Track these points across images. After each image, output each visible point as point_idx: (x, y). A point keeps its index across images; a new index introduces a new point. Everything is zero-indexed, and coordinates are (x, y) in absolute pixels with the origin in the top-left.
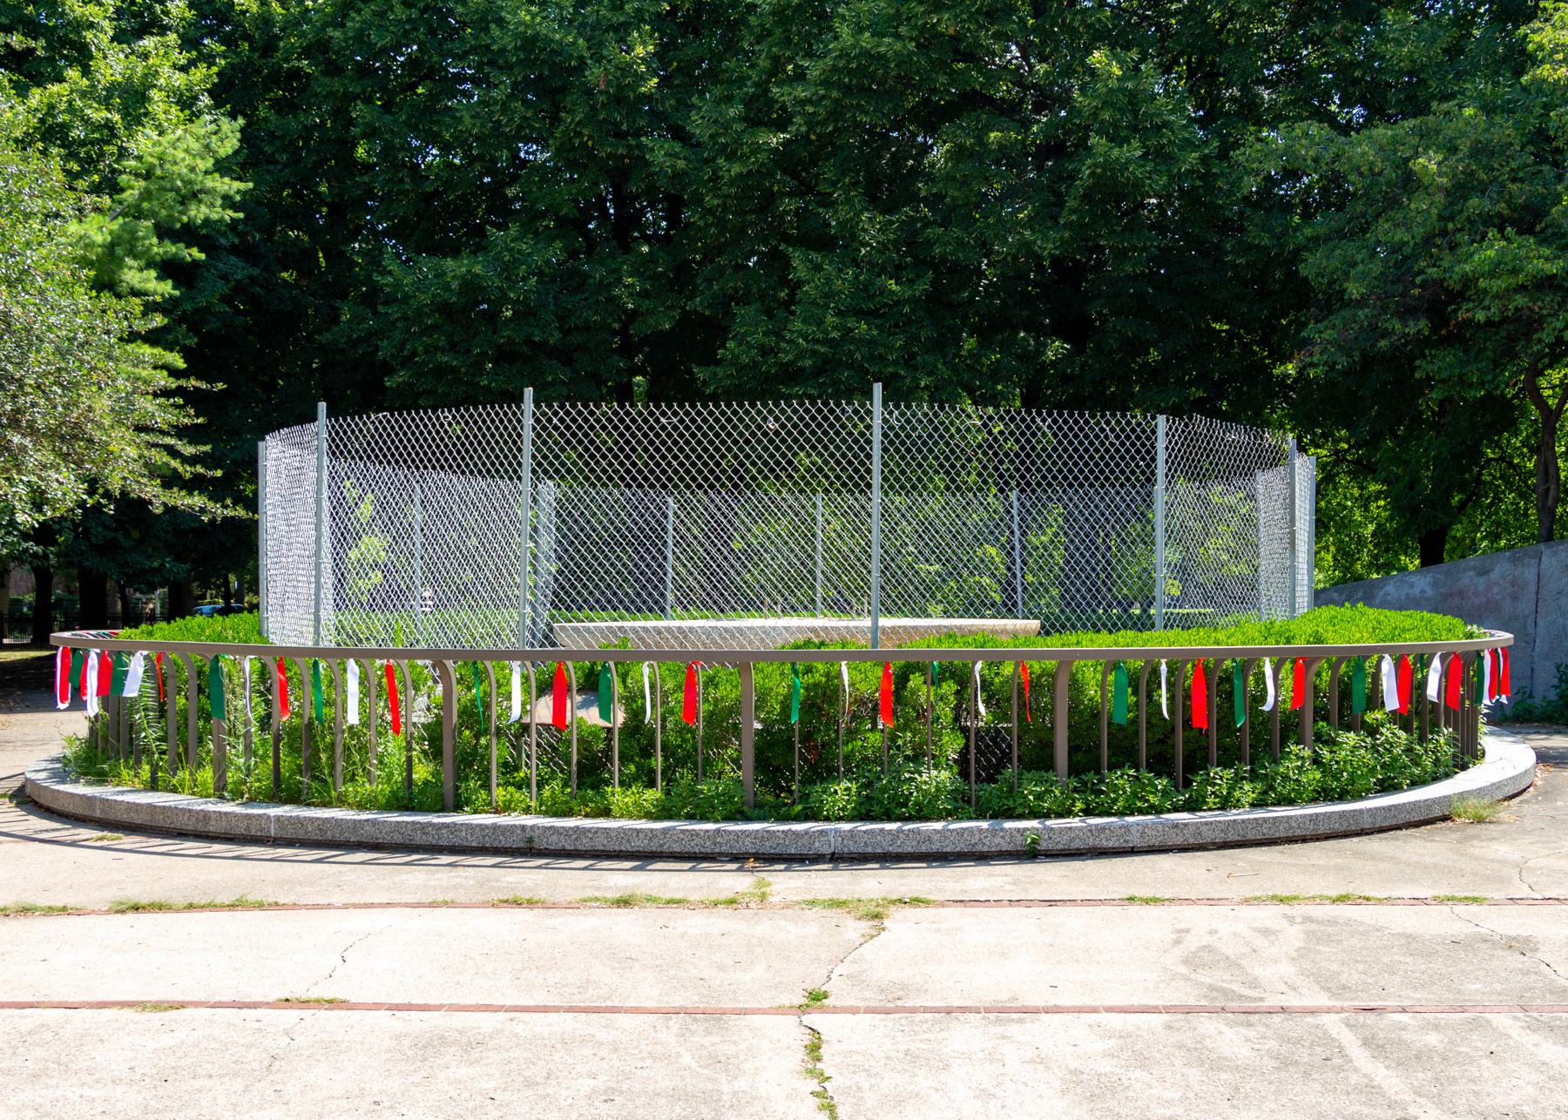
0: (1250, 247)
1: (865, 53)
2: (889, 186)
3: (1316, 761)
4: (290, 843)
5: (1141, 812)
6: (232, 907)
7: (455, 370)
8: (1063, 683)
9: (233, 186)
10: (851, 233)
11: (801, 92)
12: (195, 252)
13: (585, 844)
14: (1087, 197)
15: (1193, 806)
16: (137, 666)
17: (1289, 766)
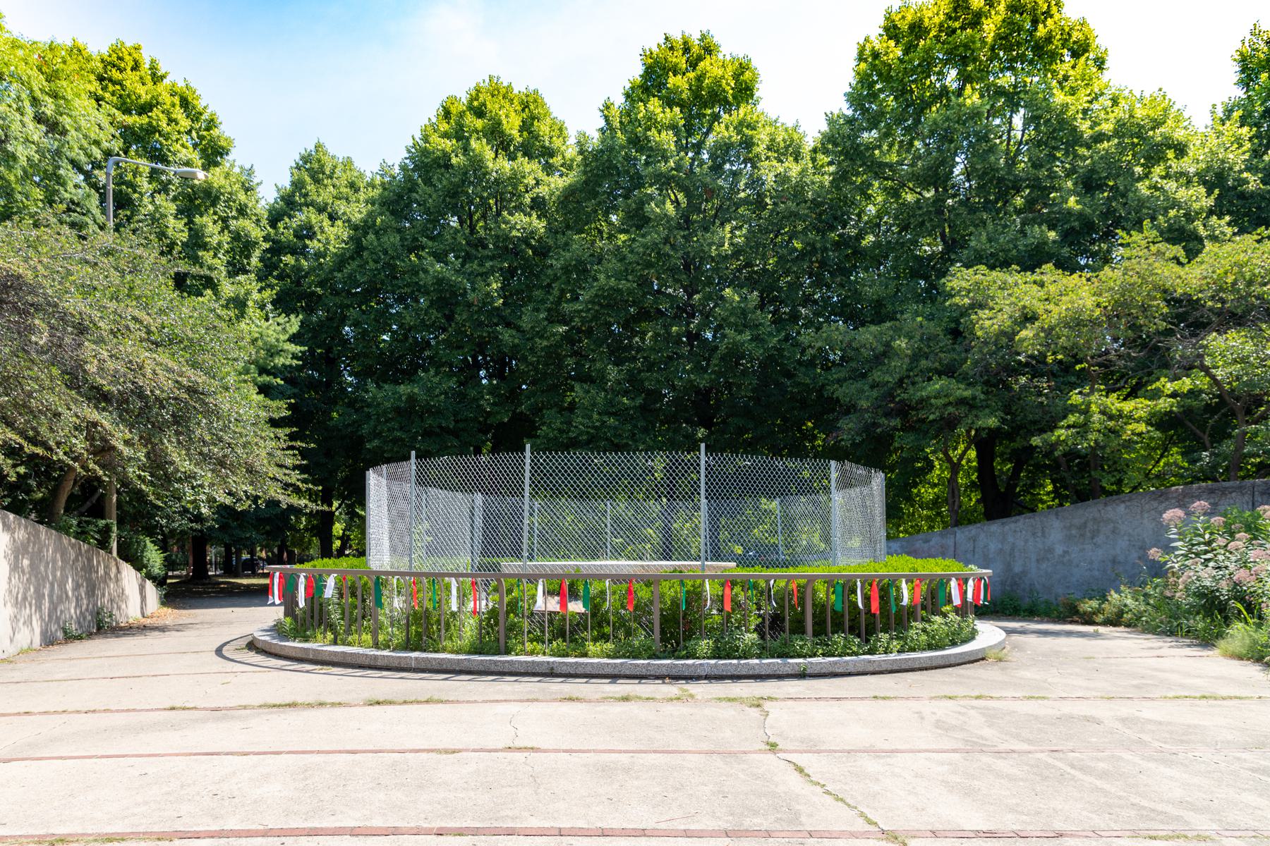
0: (800, 383)
1: (612, 288)
2: (619, 354)
3: (924, 630)
4: (423, 671)
5: (849, 655)
6: (427, 702)
7: (402, 440)
8: (809, 591)
9: (297, 349)
10: (603, 378)
11: (578, 307)
12: (279, 380)
13: (580, 671)
14: (722, 359)
15: (872, 652)
16: (331, 582)
17: (912, 632)
